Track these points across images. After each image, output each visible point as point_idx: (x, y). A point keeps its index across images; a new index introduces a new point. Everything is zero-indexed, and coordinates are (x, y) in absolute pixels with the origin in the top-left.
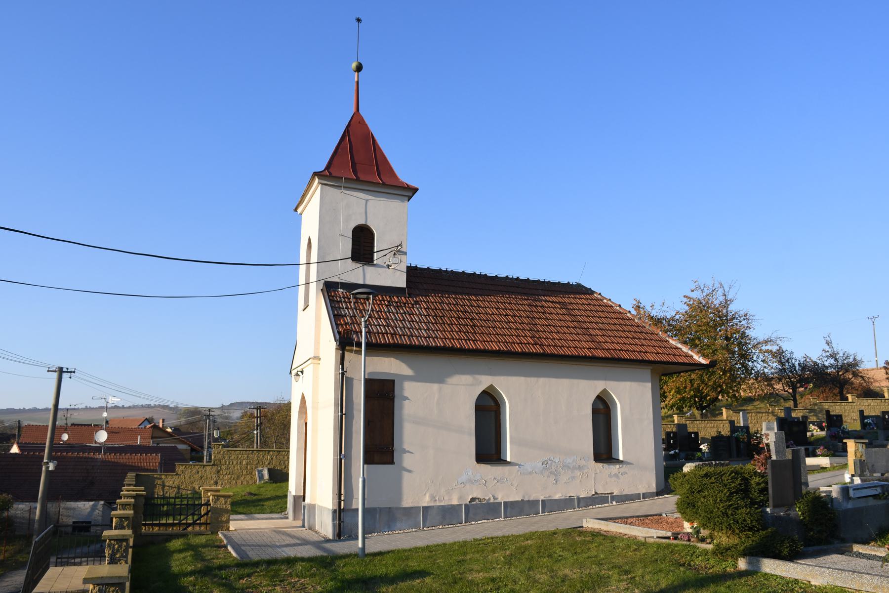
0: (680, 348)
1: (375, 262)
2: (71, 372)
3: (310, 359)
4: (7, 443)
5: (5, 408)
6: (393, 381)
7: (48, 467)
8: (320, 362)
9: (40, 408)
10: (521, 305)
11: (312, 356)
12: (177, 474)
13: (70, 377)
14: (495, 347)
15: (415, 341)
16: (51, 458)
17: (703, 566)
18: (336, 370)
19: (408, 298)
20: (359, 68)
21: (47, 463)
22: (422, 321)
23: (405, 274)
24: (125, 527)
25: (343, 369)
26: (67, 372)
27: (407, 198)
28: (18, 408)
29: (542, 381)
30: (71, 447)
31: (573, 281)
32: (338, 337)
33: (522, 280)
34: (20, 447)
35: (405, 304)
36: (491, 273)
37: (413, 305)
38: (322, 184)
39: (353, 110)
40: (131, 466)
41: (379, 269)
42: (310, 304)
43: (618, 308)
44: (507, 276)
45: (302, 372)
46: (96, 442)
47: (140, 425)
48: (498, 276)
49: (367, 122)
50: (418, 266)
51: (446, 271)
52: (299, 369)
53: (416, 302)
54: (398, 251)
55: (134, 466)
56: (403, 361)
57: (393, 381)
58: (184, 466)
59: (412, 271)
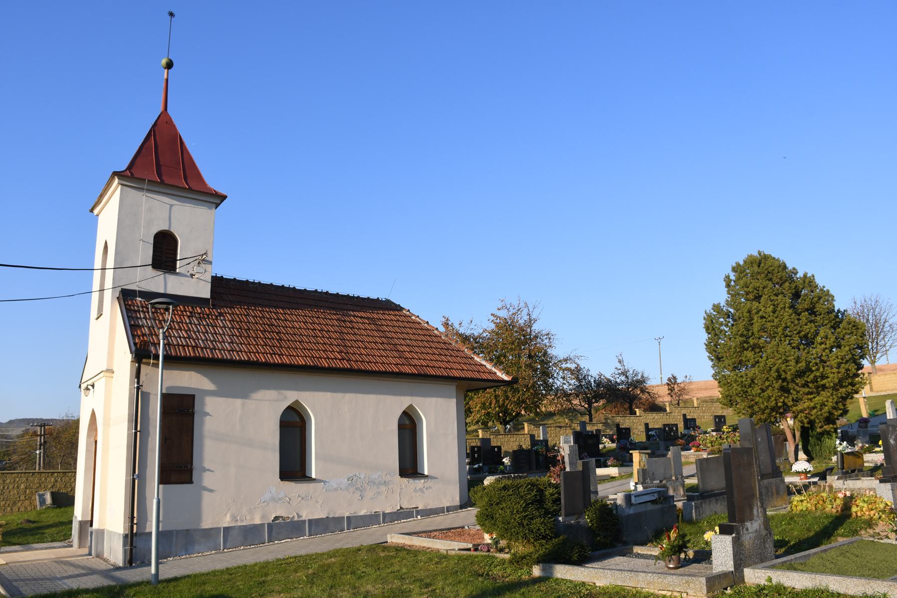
0: (484, 365)
1: (178, 271)
3: (101, 372)
6: (193, 396)
8: (114, 375)
10: (330, 320)
11: (104, 369)
13: (489, 320)
14: (301, 362)
15: (199, 353)
18: (131, 383)
19: (212, 309)
23: (209, 285)
25: (138, 383)
27: (214, 205)
29: (348, 396)
31: (383, 296)
33: (331, 294)
35: (208, 315)
36: (300, 286)
37: (216, 316)
38: (122, 185)
39: (161, 109)
42: (104, 313)
43: (426, 325)
45: (93, 386)
50: (224, 277)
51: (254, 283)
53: (221, 314)
54: (203, 260)
57: (193, 396)
59: (218, 282)
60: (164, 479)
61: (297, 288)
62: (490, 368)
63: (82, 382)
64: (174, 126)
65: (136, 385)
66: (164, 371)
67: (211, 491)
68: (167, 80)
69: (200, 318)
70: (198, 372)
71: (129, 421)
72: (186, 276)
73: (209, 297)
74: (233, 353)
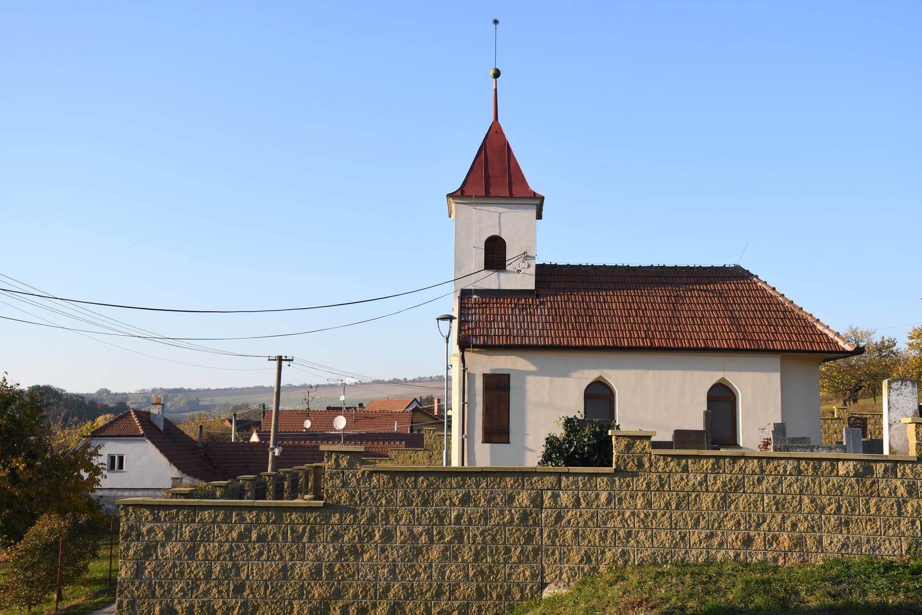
0: (825, 334)
1: (507, 268)
2: (289, 360)
4: (247, 431)
5: (253, 386)
6: (509, 375)
7: (274, 453)
9: (297, 385)
10: (659, 296)
12: (390, 459)
13: (289, 365)
14: (601, 342)
15: (511, 341)
16: (276, 445)
18: (460, 368)
19: (536, 299)
20: (497, 74)
21: (273, 449)
23: (534, 277)
24: (277, 471)
25: (464, 366)
26: (286, 360)
28: (269, 386)
29: (651, 372)
30: (314, 435)
31: (730, 262)
34: (259, 436)
35: (530, 305)
36: (634, 263)
37: (537, 306)
39: (492, 119)
44: (652, 265)
46: (335, 430)
47: (407, 408)
48: (642, 266)
49: (504, 131)
51: (587, 266)
53: (541, 303)
56: (528, 360)
57: (509, 375)
58: (397, 451)
59: (545, 273)
60: (487, 439)
61: (630, 266)
62: (832, 337)
64: (503, 134)
66: (468, 355)
67: (532, 451)
68: (496, 90)
69: (523, 309)
72: (513, 272)
73: (534, 288)
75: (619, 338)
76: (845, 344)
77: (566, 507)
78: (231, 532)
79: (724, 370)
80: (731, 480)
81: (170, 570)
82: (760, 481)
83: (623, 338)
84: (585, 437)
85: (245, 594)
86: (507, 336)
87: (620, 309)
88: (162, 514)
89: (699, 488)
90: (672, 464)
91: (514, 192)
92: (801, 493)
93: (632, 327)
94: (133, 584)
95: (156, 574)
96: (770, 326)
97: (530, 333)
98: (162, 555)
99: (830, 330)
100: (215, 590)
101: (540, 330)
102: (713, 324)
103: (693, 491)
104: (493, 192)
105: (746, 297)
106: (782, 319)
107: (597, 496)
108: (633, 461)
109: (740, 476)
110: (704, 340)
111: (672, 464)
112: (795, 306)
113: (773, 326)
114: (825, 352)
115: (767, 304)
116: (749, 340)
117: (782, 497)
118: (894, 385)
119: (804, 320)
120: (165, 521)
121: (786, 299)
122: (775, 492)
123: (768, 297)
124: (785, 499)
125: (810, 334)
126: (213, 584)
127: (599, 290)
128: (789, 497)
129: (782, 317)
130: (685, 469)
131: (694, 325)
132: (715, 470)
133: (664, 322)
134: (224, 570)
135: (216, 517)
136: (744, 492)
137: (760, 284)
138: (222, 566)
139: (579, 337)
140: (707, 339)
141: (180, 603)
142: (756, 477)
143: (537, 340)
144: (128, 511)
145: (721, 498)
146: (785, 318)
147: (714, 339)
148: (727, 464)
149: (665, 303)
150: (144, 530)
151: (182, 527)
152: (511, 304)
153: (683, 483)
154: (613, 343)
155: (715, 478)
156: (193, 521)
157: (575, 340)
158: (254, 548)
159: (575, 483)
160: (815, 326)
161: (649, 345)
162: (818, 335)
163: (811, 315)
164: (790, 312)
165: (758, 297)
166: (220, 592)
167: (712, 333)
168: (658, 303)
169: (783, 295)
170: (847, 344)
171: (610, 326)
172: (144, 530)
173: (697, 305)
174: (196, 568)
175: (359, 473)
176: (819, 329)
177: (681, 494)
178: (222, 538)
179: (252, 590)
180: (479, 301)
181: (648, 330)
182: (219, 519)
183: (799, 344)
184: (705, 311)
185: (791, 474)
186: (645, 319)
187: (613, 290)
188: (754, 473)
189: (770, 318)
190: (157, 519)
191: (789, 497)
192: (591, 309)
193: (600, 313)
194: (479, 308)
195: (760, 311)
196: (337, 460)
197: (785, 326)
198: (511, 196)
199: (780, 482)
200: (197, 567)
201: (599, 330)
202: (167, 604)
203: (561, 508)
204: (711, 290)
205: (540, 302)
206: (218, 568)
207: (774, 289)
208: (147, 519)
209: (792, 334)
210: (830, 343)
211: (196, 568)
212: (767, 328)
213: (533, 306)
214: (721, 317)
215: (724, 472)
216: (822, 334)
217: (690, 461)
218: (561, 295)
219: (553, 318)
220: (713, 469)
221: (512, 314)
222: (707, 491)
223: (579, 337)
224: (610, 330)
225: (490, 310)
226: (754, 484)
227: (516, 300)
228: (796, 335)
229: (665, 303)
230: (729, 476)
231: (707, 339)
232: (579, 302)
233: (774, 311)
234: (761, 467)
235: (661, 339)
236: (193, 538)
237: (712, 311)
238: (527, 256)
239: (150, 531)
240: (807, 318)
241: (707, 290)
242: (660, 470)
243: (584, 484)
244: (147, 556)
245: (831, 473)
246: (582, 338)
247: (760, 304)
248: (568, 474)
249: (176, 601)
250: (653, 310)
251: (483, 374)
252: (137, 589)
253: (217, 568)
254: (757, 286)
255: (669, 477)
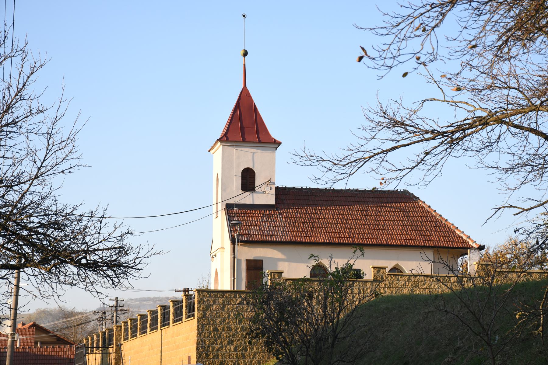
6: (262, 261)
8: (225, 250)
10: (355, 210)
11: (220, 247)
14: (321, 240)
15: (274, 239)
17: (388, 335)
18: (231, 255)
19: (276, 211)
20: (245, 54)
22: (281, 226)
23: (274, 196)
27: (275, 148)
32: (231, 238)
33: (361, 191)
35: (273, 215)
37: (277, 215)
38: (222, 145)
40: (44, 355)
41: (258, 194)
42: (218, 216)
43: (428, 208)
44: (349, 189)
45: (216, 256)
50: (287, 187)
51: (306, 189)
52: (214, 254)
53: (280, 214)
54: (269, 182)
55: (48, 355)
57: (262, 261)
59: (281, 192)
62: (465, 239)
63: (212, 252)
64: (251, 97)
65: (233, 256)
68: (245, 65)
69: (268, 217)
70: (271, 248)
71: (231, 269)
72: (260, 193)
74: (283, 237)
75: (332, 237)
76: (473, 243)
77: (356, 293)
78: (236, 301)
79: (398, 259)
80: (414, 284)
81: (215, 314)
82: (424, 284)
83: (335, 237)
84: (350, 275)
85: (242, 323)
86: (261, 235)
87: (331, 218)
88: (212, 294)
89: (403, 286)
90: (393, 278)
91: (261, 139)
92: (438, 288)
93: (340, 230)
94: (203, 319)
95: (211, 316)
96: (427, 231)
97: (276, 233)
98: (212, 309)
99: (464, 234)
100: (232, 322)
101: (281, 231)
102: (391, 230)
103: (401, 288)
104: (246, 136)
105: (411, 212)
106: (434, 227)
107: (367, 289)
108: (380, 277)
109: (417, 282)
110: (385, 239)
111: (393, 278)
112: (443, 218)
113: (429, 231)
114: (460, 248)
115: (425, 217)
116: (413, 240)
117: (432, 290)
118: (472, 251)
119: (448, 228)
120: (213, 297)
121: (437, 214)
122: (429, 288)
123: (425, 212)
124: (433, 290)
125: (452, 237)
126: (231, 320)
127: (317, 205)
128: (435, 290)
129: (435, 225)
130: (398, 280)
131: (379, 230)
132: (409, 280)
133: (360, 227)
134: (235, 315)
135: (231, 295)
136: (419, 288)
137: (420, 203)
138: (234, 313)
139: (307, 237)
140: (387, 239)
141: (219, 326)
142: (423, 283)
143: (285, 238)
144: (200, 293)
145: (411, 290)
146: (436, 226)
147: (392, 239)
148: (413, 278)
149: (360, 215)
150: (206, 300)
151: (219, 299)
152: (260, 214)
153: (397, 285)
154: (329, 240)
155: (408, 283)
156: (223, 297)
157: (305, 238)
158: (245, 307)
159: (359, 284)
160: (455, 232)
161: (351, 242)
162: (457, 237)
163: (453, 224)
164: (439, 222)
165: (419, 212)
166: (233, 323)
167: (391, 235)
168: (355, 215)
169: (435, 211)
170: (474, 244)
171: (326, 230)
172: (206, 300)
173: (404, 217)
174: (224, 314)
175: (282, 280)
176: (457, 234)
177: (397, 289)
178: (234, 303)
179: (245, 322)
180: (239, 212)
181: (350, 233)
182: (232, 296)
183: (445, 243)
184: (385, 220)
185: (435, 282)
186: (347, 226)
187: (325, 205)
188: (422, 281)
189: (427, 226)
190: (210, 296)
191: (435, 290)
192: (312, 218)
193: (318, 221)
194: (240, 216)
195: (421, 222)
196: (274, 276)
197: (436, 231)
198: (260, 142)
199: (431, 285)
200: (225, 314)
201: (319, 232)
202: (215, 327)
203: (354, 293)
204: (394, 207)
205: (279, 213)
206: (233, 314)
207: (429, 207)
208: (206, 296)
209: (440, 236)
210: (464, 243)
211: (224, 314)
212: (425, 232)
213: (275, 215)
214: (396, 225)
215: (412, 281)
216: (459, 236)
217: (400, 277)
218: (292, 209)
219: (289, 224)
220: (408, 280)
221: (262, 221)
222: (406, 287)
223: (307, 237)
224: (326, 232)
225: (247, 218)
226: (422, 285)
227: (249, 211)
228: (443, 237)
229: (360, 215)
230: (413, 282)
231: (387, 239)
232: (304, 213)
233: (429, 221)
234: (425, 279)
235: (359, 238)
236: (223, 303)
237: (390, 221)
238: (271, 182)
239: (208, 300)
240: (450, 227)
241: (391, 207)
242: (389, 280)
243: (362, 285)
244: (207, 310)
245: (449, 281)
246: (309, 237)
247: (420, 216)
248: (357, 281)
249: (218, 326)
250: (352, 220)
251: (246, 260)
252: (204, 321)
253: (232, 314)
254: (418, 204)
255: (392, 282)
